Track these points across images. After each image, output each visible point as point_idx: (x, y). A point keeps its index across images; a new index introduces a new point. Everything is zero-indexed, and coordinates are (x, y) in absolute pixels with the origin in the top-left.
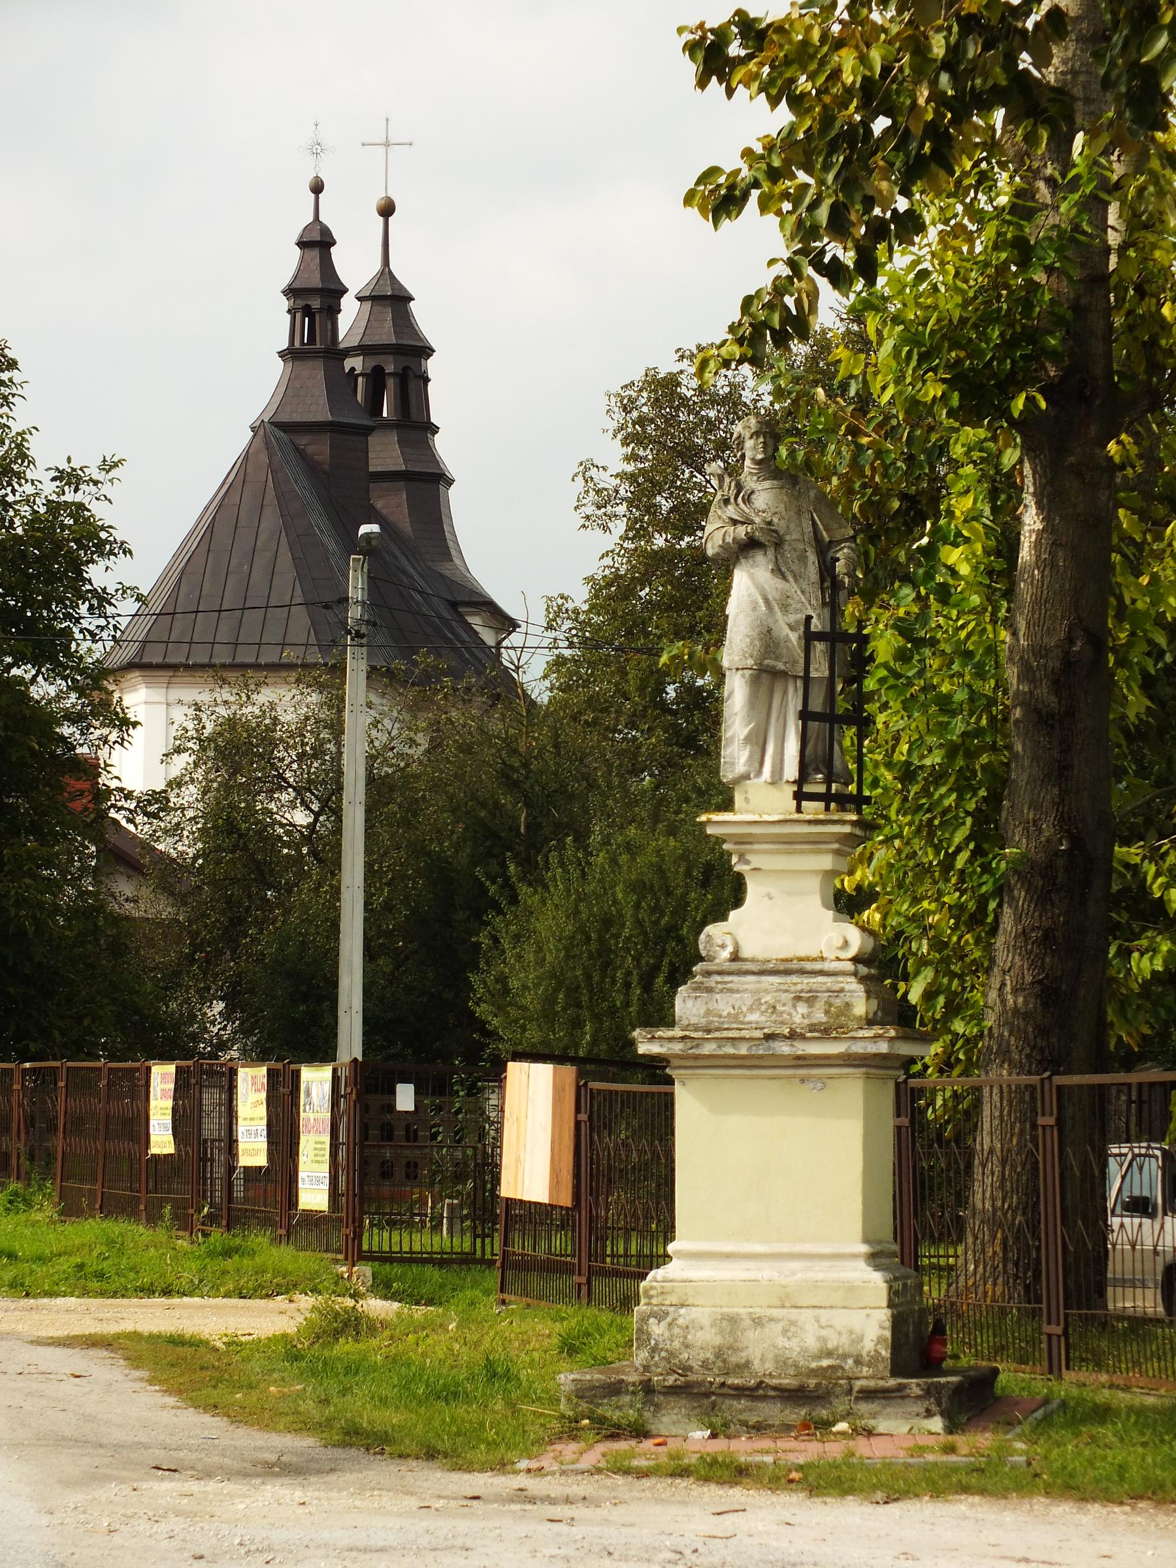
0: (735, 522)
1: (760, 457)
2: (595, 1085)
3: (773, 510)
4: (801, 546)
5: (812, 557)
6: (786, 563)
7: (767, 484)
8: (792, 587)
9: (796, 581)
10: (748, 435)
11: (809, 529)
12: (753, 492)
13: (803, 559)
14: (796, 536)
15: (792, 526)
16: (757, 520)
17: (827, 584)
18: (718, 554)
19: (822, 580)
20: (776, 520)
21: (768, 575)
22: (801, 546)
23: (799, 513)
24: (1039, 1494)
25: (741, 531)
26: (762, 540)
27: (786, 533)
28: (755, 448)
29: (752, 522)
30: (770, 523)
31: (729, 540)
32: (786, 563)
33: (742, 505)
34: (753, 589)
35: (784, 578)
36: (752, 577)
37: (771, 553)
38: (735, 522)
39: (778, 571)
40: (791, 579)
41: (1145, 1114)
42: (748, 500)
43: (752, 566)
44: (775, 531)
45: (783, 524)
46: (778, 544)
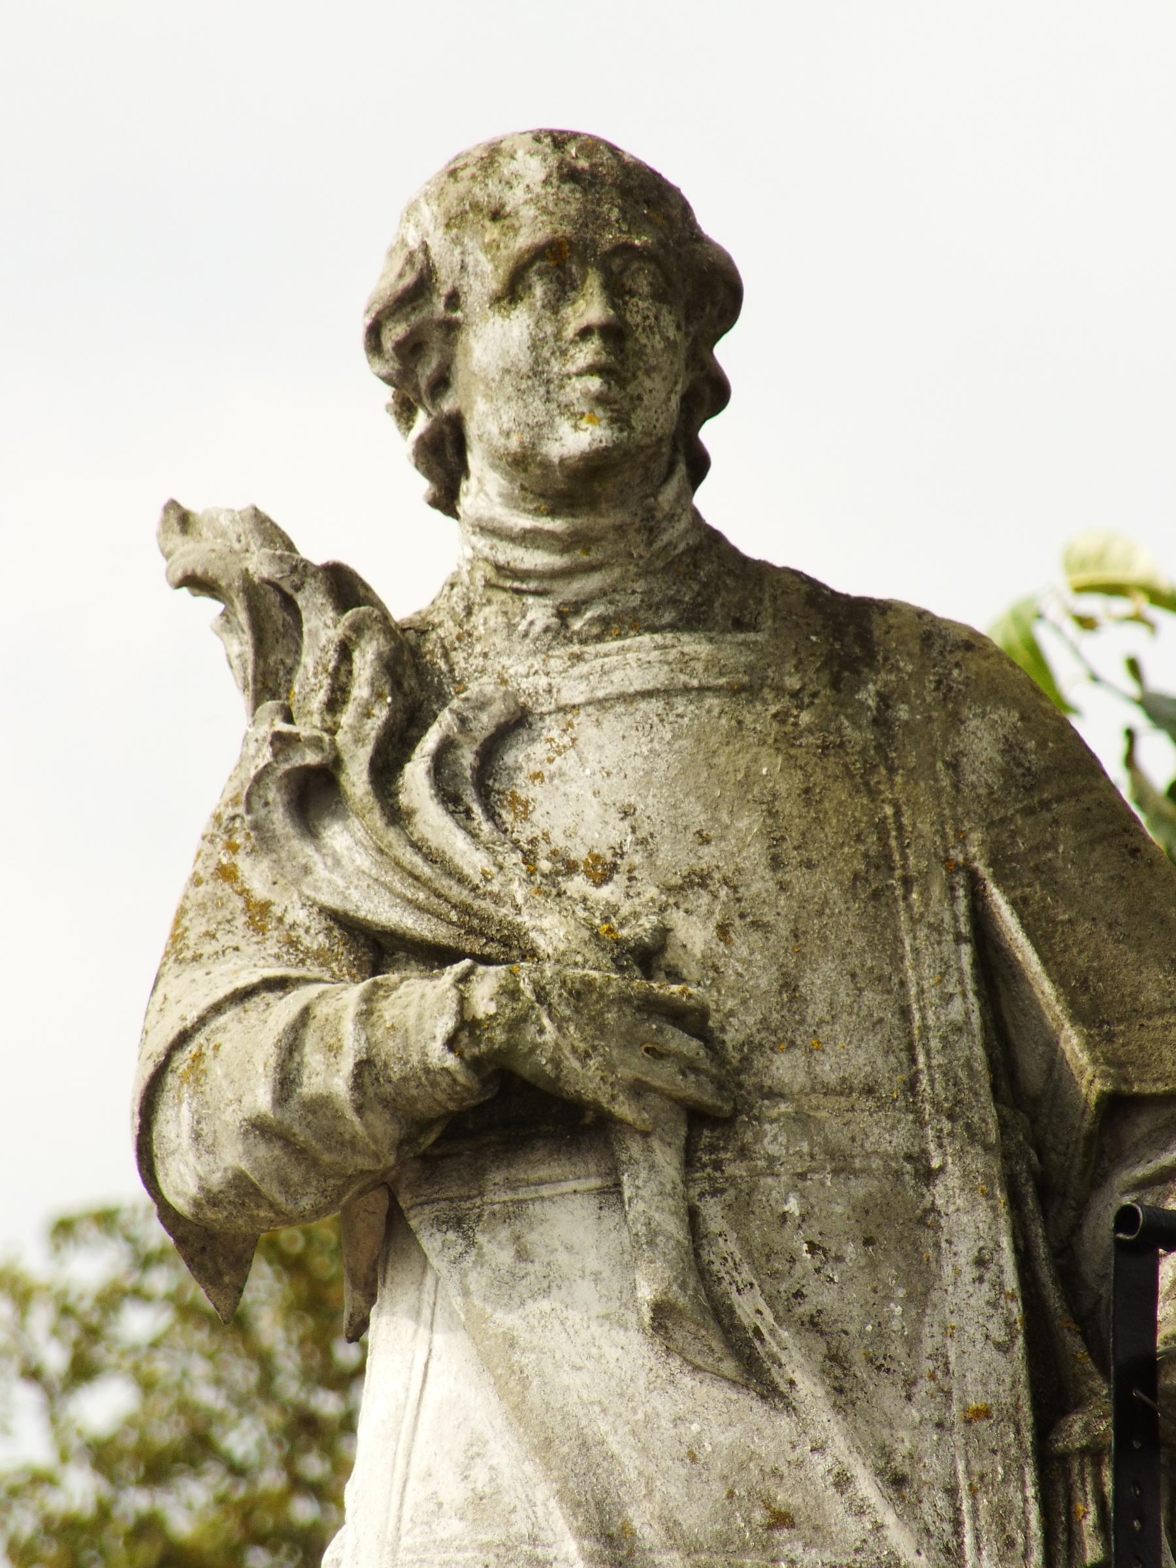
0: (375, 950)
1: (575, 439)
2: (1121, 1235)
3: (675, 857)
4: (887, 1136)
5: (971, 1220)
6: (766, 1261)
7: (635, 661)
8: (813, 1444)
9: (843, 1395)
10: (484, 276)
11: (948, 1003)
12: (518, 722)
13: (899, 1229)
14: (851, 1056)
15: (822, 980)
16: (550, 930)
17: (1090, 1424)
18: (242, 1188)
19: (1051, 1397)
20: (693, 934)
21: (629, 1351)
22: (887, 1136)
23: (878, 882)
24: (397, 802)
25: (422, 1013)
26: (587, 1078)
27: (777, 1037)
28: (537, 375)
29: (511, 946)
30: (649, 956)
31: (329, 1076)
32: (766, 1261)
33: (432, 820)
34: (507, 1459)
35: (753, 1372)
36: (503, 1367)
37: (652, 1179)
38: (375, 950)
39: (705, 1323)
40: (809, 1388)
41: (392, 1523)
42: (480, 781)
43: (507, 1288)
44: (692, 1019)
45: (752, 964)
46: (713, 1123)
